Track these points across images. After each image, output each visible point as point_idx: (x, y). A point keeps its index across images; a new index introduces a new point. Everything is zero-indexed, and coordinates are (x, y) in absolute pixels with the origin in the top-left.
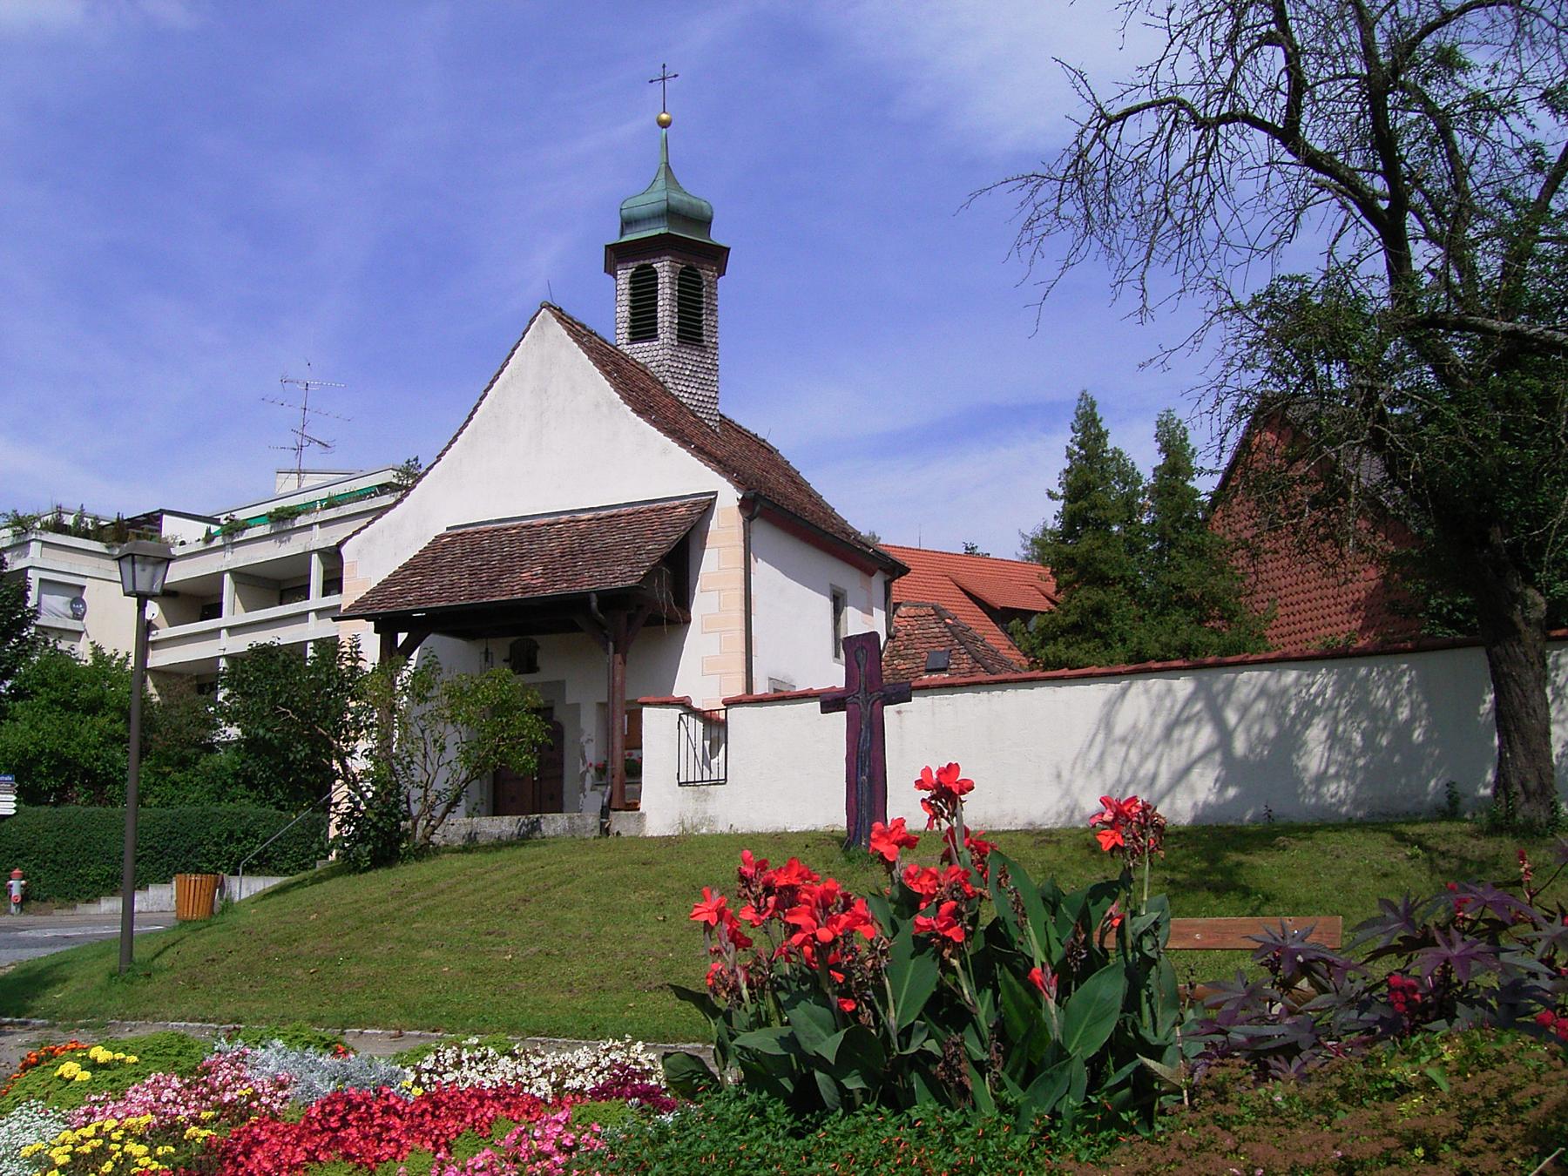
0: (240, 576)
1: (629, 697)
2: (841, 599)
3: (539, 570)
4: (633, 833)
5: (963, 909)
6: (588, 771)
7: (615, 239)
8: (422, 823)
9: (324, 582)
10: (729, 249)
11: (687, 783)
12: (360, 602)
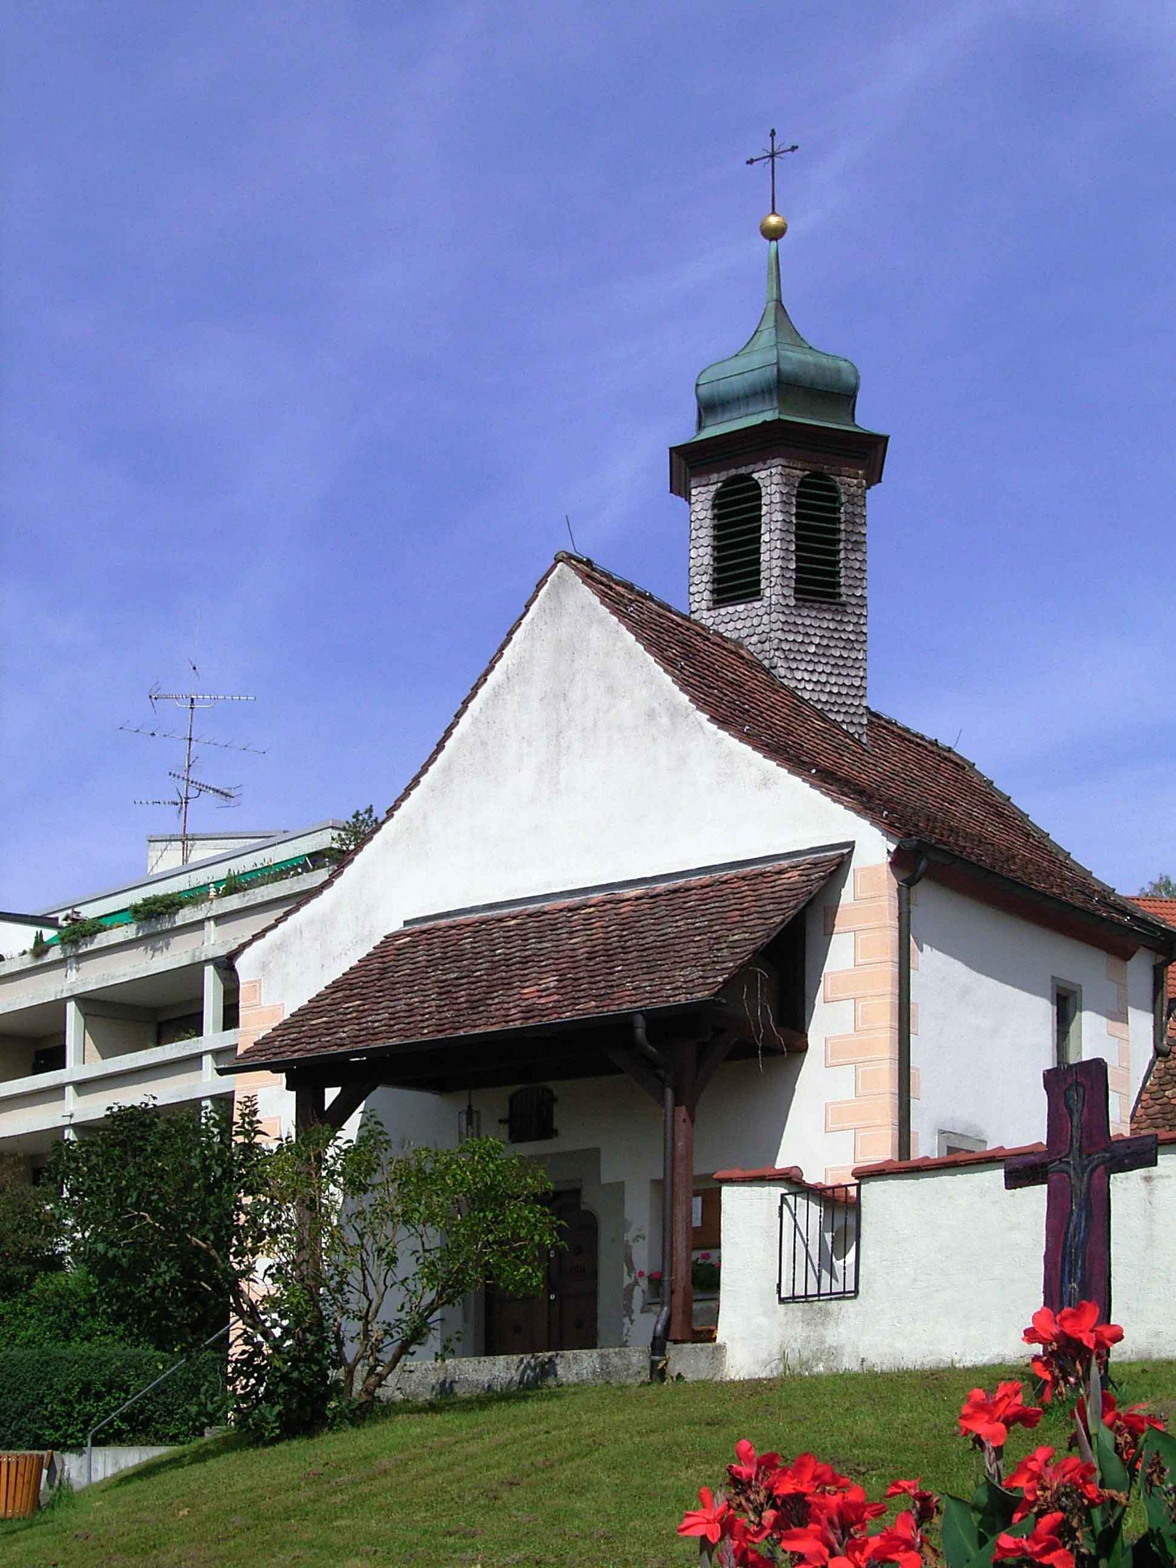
0: (91, 1004)
1: (700, 1169)
2: (1071, 1001)
3: (551, 981)
4: (702, 1377)
5: (1075, 1524)
6: (636, 1283)
8: (361, 1371)
9: (224, 1007)
10: (885, 439)
11: (794, 1298)
12: (264, 1044)
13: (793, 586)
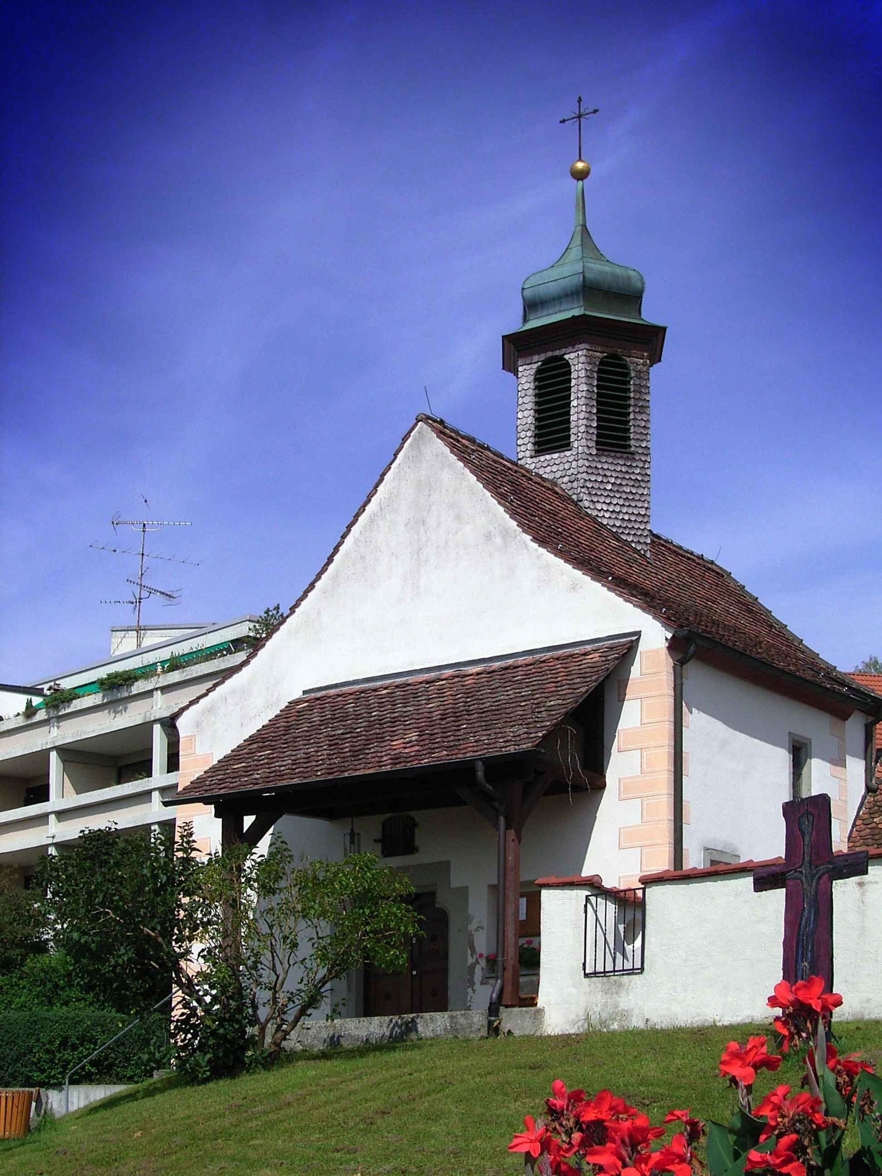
0: (68, 753)
1: (525, 877)
2: (803, 751)
3: (413, 736)
4: (527, 1033)
5: (806, 1143)
6: (477, 962)
7: (515, 325)
8: (271, 1028)
9: (168, 755)
10: (664, 330)
11: (595, 974)
12: (198, 783)
13: (595, 439)
